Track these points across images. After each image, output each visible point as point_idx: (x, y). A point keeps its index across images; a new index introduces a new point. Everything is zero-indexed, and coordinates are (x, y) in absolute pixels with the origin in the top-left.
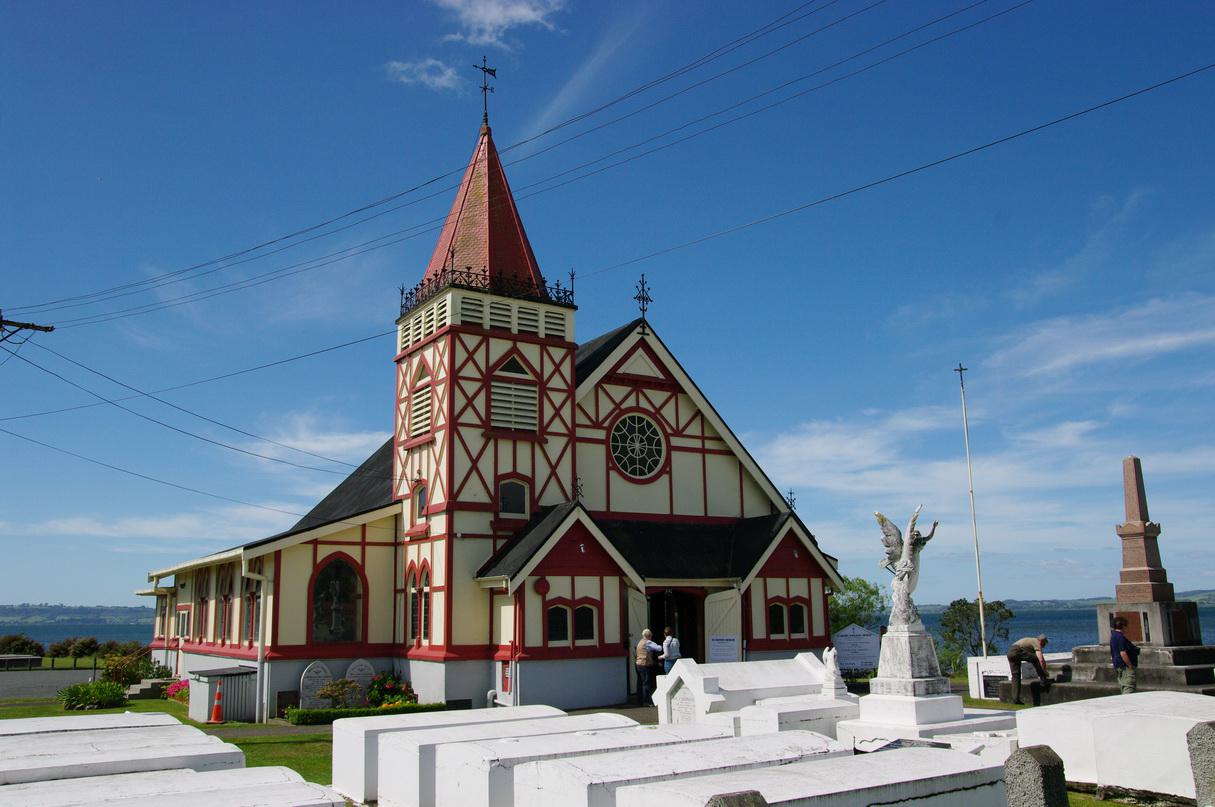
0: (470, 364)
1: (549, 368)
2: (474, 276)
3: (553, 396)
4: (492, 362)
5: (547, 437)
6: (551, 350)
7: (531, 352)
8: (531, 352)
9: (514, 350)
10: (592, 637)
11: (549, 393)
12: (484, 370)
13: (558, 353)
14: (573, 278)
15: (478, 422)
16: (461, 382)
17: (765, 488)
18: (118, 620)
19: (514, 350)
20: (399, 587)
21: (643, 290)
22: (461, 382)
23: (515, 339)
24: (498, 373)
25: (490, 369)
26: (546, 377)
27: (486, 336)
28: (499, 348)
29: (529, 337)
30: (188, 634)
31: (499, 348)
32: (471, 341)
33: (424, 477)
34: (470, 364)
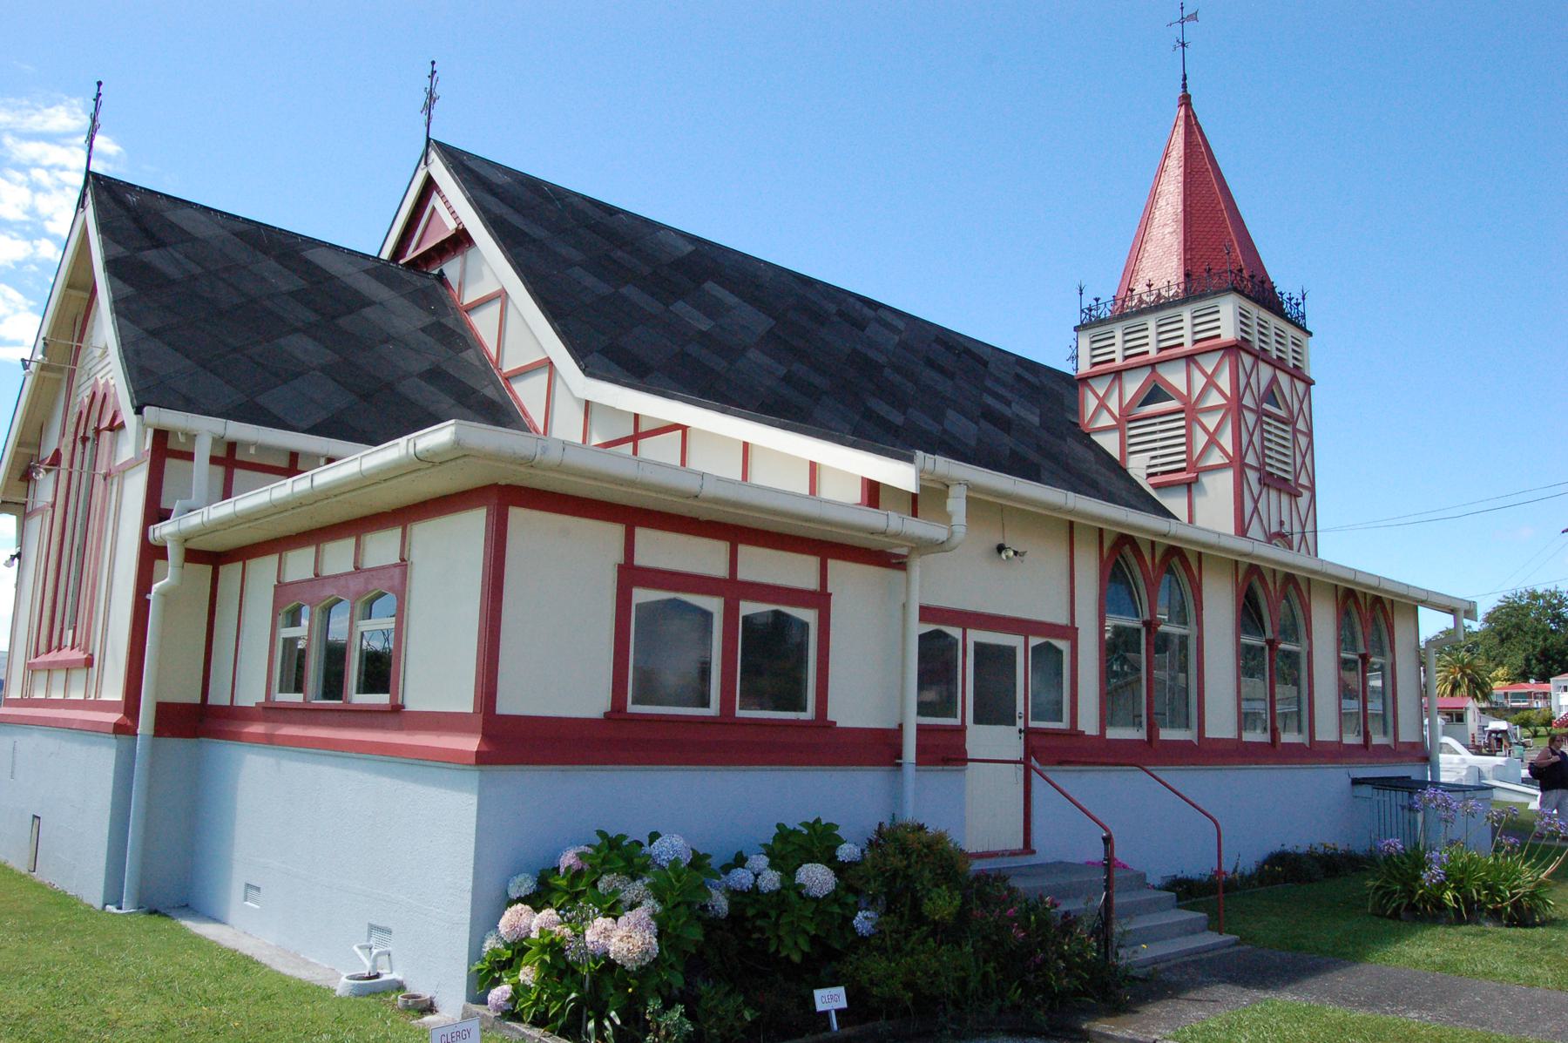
15: (1224, 402)
27: (1118, 374)
28: (1133, 385)
33: (1286, 528)
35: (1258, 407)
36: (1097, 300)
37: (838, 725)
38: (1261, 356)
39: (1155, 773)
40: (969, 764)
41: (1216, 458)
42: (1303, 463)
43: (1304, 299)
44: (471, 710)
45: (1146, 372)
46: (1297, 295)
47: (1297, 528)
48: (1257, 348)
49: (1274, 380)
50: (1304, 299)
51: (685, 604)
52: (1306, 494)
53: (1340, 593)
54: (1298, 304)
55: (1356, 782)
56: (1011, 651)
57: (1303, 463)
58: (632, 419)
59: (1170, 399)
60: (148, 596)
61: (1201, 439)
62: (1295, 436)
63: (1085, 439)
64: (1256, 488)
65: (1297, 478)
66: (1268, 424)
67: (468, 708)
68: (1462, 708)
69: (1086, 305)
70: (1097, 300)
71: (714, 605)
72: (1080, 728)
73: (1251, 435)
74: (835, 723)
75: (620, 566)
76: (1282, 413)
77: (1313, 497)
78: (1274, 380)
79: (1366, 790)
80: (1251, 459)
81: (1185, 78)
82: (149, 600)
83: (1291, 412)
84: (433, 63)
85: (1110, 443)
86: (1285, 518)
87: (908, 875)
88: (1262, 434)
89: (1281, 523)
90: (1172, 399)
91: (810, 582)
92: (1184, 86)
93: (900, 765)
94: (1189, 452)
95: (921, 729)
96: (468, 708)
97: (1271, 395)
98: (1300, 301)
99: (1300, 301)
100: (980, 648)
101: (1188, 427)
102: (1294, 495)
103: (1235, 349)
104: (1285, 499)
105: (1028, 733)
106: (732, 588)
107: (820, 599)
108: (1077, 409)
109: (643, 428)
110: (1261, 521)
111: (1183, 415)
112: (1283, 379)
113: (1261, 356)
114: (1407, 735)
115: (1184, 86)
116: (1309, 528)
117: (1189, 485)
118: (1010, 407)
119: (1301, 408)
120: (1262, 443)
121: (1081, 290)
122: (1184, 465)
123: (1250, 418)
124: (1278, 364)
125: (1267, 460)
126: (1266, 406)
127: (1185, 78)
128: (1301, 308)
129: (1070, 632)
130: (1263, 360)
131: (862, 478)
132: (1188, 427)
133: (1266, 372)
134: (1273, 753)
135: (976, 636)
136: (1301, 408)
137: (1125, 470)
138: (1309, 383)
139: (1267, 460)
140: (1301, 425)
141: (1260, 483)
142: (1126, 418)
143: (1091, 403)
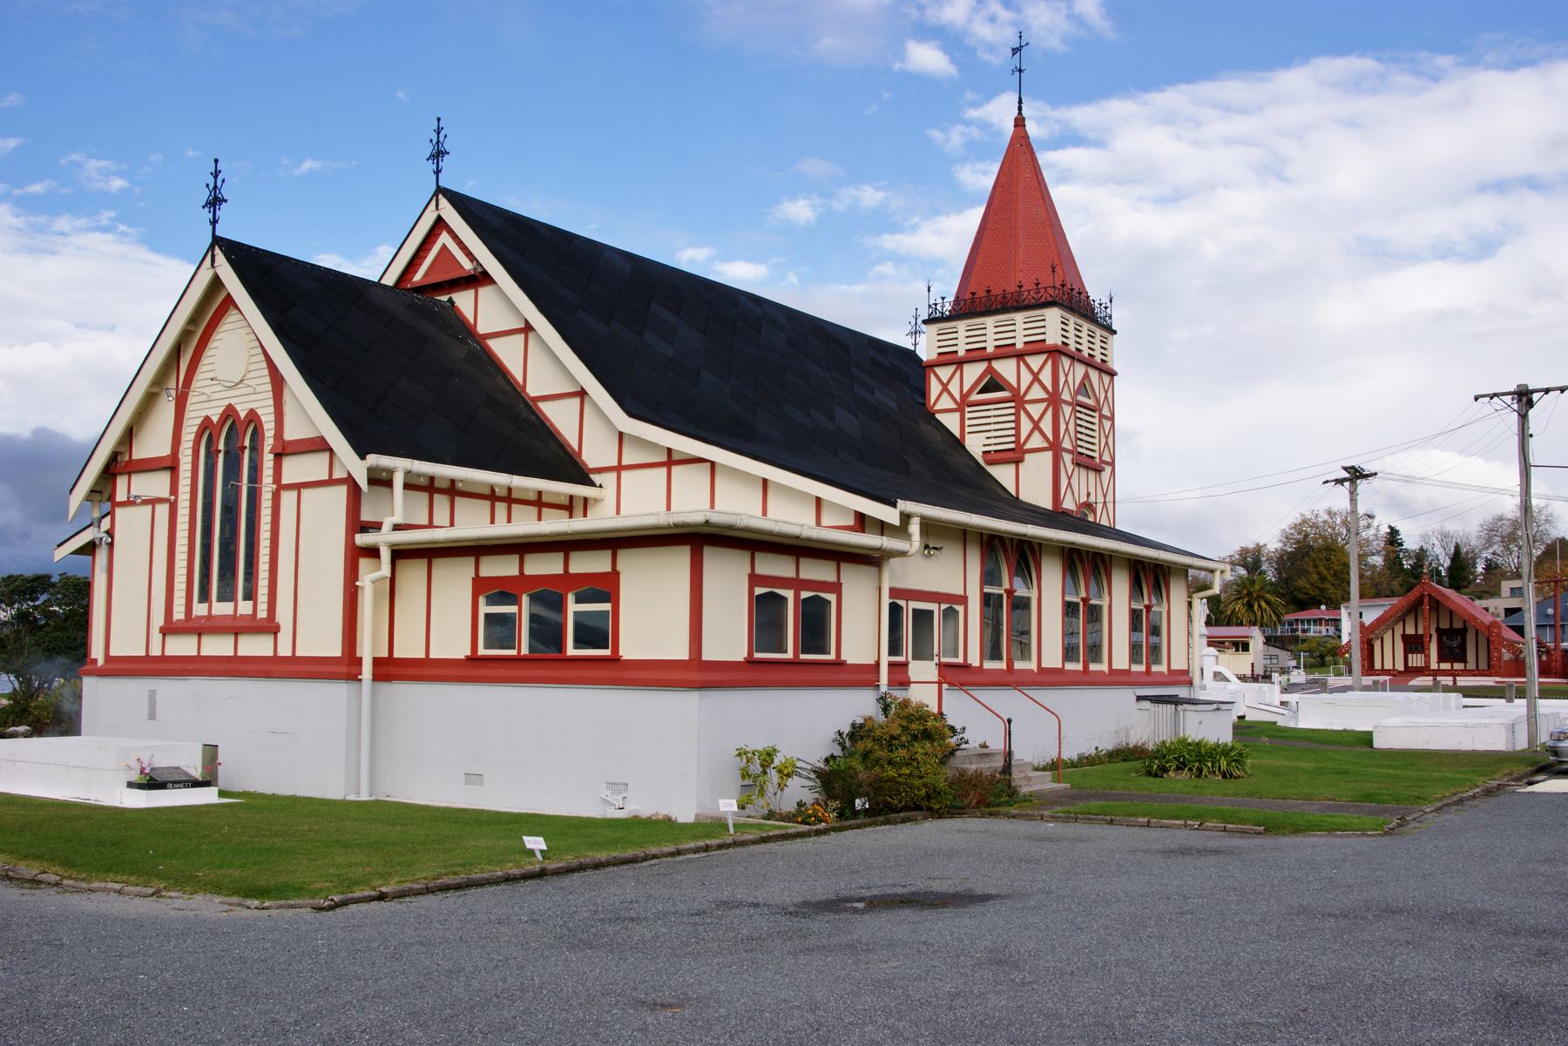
0: (1036, 386)
1: (1026, 378)
2: (1042, 291)
3: (1032, 409)
5: (238, 615)
6: (1029, 359)
7: (1006, 369)
8: (1006, 369)
9: (990, 370)
10: (914, 610)
11: (1027, 406)
12: (958, 398)
13: (1035, 362)
14: (929, 291)
16: (1027, 406)
17: (1550, 687)
18: (548, 425)
19: (990, 370)
20: (664, 458)
21: (916, 324)
22: (1027, 406)
23: (989, 359)
24: (975, 397)
25: (964, 397)
26: (1023, 390)
27: (960, 363)
28: (973, 372)
29: (1005, 352)
30: (901, 530)
31: (973, 372)
32: (944, 373)
33: (1092, 499)
34: (1036, 386)
35: (1073, 399)
36: (943, 298)
38: (1075, 357)
39: (1025, 691)
40: (912, 685)
42: (1107, 443)
43: (1111, 302)
44: (339, 654)
45: (983, 366)
46: (1105, 300)
47: (1100, 499)
48: (1074, 350)
50: (1111, 302)
51: (776, 594)
52: (1108, 469)
53: (1132, 563)
54: (1106, 308)
55: (1139, 698)
56: (931, 613)
57: (1107, 443)
59: (1002, 389)
61: (1026, 426)
62: (1100, 422)
63: (930, 416)
64: (1070, 467)
65: (1101, 456)
66: (1080, 412)
67: (338, 653)
68: (1248, 637)
69: (932, 302)
70: (943, 298)
71: (789, 594)
72: (843, 658)
73: (1067, 424)
75: (749, 575)
76: (1091, 402)
77: (1113, 470)
78: (1086, 376)
79: (1146, 704)
80: (1067, 444)
83: (1098, 401)
84: (439, 119)
85: (951, 422)
86: (1092, 491)
88: (1075, 421)
89: (1088, 495)
90: (1005, 390)
91: (832, 578)
92: (1020, 109)
93: (878, 686)
94: (1017, 435)
95: (891, 665)
96: (338, 653)
97: (1084, 387)
98: (1108, 304)
99: (1108, 304)
102: (1098, 471)
103: (1057, 353)
104: (1092, 475)
105: (941, 666)
106: (797, 584)
107: (836, 588)
108: (923, 392)
109: (675, 457)
110: (1073, 494)
111: (1013, 404)
112: (1094, 375)
113: (1075, 357)
114: (1178, 664)
115: (1020, 109)
116: (1109, 498)
118: (874, 394)
119: (1106, 397)
120: (1076, 429)
121: (929, 288)
122: (1012, 446)
123: (1067, 410)
124: (1089, 363)
125: (1079, 443)
126: (1081, 398)
128: (1108, 311)
129: (963, 600)
130: (1078, 360)
131: (855, 511)
132: (1017, 415)
133: (1080, 370)
134: (1086, 680)
135: (914, 605)
136: (1106, 397)
137: (964, 447)
138: (1112, 374)
139: (1079, 443)
140: (1106, 412)
141: (1073, 463)
142: (963, 404)
143: (935, 388)
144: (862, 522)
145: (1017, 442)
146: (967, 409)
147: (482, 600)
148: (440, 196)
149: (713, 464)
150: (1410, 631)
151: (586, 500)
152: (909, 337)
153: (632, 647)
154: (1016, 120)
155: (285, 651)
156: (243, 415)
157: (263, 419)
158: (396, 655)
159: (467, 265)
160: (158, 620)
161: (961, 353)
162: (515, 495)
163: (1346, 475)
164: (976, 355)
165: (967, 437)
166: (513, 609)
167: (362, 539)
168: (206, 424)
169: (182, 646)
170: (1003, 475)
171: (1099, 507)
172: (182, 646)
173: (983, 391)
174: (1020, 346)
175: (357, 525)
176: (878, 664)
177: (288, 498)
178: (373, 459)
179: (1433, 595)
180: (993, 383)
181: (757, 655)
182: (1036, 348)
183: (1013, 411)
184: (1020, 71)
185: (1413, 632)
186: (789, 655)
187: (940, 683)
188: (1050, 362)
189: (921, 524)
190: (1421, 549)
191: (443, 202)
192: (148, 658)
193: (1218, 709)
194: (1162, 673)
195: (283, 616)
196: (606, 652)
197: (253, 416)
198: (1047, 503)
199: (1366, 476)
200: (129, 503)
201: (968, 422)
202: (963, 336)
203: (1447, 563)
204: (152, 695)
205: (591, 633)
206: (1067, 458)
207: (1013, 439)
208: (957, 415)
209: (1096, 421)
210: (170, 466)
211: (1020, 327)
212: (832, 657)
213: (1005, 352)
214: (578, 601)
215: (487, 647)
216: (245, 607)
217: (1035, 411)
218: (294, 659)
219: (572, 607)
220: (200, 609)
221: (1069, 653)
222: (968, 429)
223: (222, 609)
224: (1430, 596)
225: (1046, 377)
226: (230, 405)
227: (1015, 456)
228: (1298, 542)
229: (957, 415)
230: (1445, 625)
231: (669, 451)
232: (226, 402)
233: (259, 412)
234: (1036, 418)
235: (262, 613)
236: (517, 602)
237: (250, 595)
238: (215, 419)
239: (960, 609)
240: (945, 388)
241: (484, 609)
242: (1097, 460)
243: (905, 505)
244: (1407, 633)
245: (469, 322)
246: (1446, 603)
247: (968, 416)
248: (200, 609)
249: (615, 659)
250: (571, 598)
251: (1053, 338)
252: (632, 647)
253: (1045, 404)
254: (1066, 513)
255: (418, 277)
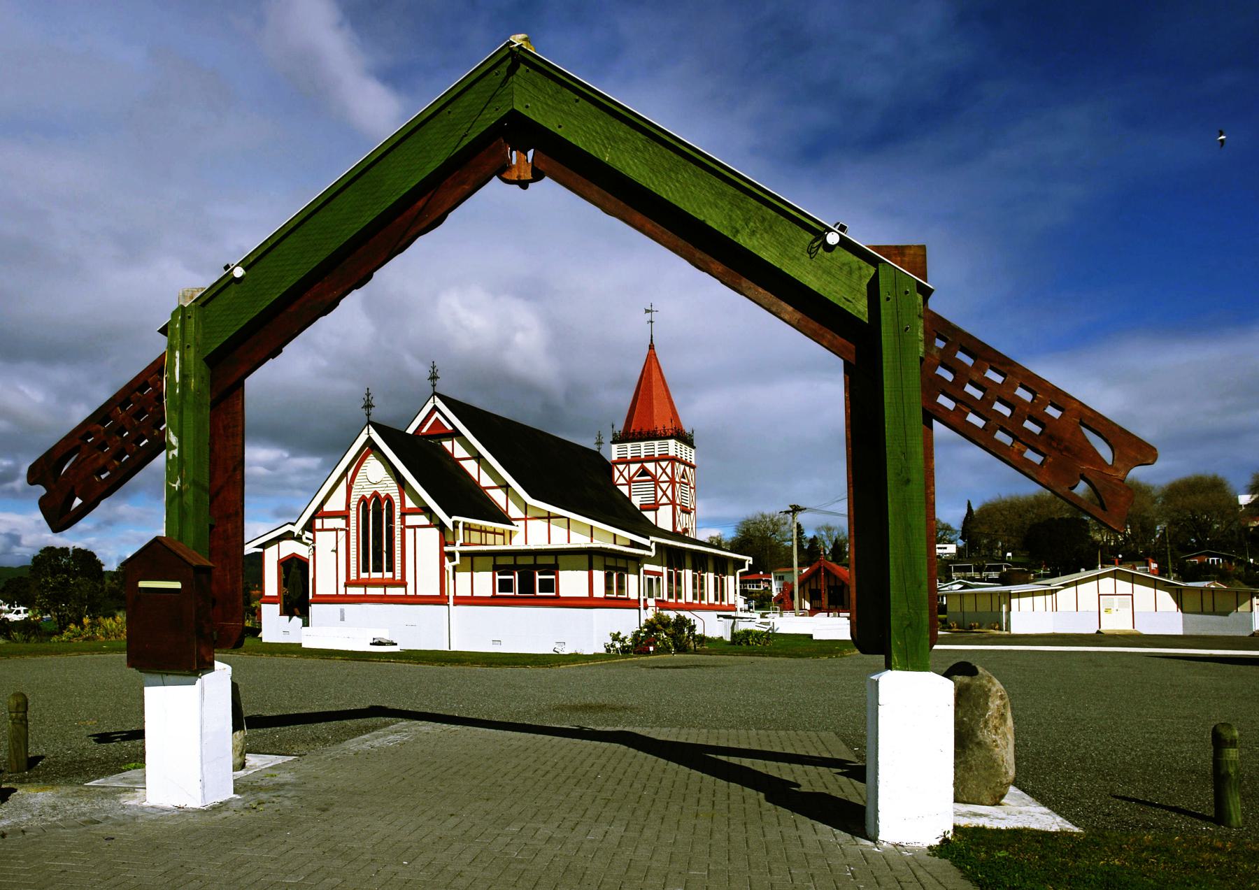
0: (664, 475)
1: (660, 471)
4: (631, 475)
6: (661, 463)
7: (650, 466)
8: (650, 466)
9: (642, 467)
12: (627, 478)
13: (664, 464)
15: (668, 480)
19: (642, 467)
23: (642, 461)
24: (635, 478)
29: (650, 459)
31: (634, 467)
32: (621, 467)
33: (687, 527)
37: (303, 646)
41: (665, 500)
45: (639, 465)
46: (691, 433)
47: (690, 527)
49: (685, 470)
55: (719, 616)
56: (652, 579)
58: (590, 528)
59: (648, 475)
60: (1083, 570)
61: (660, 493)
63: (615, 486)
64: (679, 512)
74: (300, 644)
76: (686, 481)
78: (685, 470)
79: (721, 619)
80: (678, 502)
81: (652, 337)
82: (1080, 572)
85: (625, 490)
86: (687, 522)
87: (780, 579)
91: (625, 566)
92: (652, 340)
94: (656, 497)
100: (648, 578)
101: (655, 488)
102: (689, 513)
105: (656, 600)
109: (551, 515)
111: (653, 483)
112: (687, 468)
114: (732, 602)
117: (656, 510)
122: (653, 502)
127: (652, 337)
132: (655, 488)
133: (682, 467)
142: (630, 482)
143: (617, 474)
144: (633, 544)
145: (656, 500)
146: (632, 484)
147: (497, 574)
148: (435, 397)
149: (569, 519)
150: (813, 587)
151: (511, 532)
152: (364, 409)
153: (565, 591)
154: (650, 346)
155: (411, 592)
156: (383, 496)
157: (394, 498)
158: (475, 595)
159: (450, 428)
160: (342, 580)
161: (629, 458)
162: (472, 527)
163: (791, 509)
164: (636, 460)
165: (632, 497)
166: (512, 577)
167: (446, 549)
168: (363, 499)
169: (352, 591)
170: (650, 515)
171: (690, 530)
172: (352, 591)
173: (638, 476)
174: (656, 456)
175: (443, 543)
176: (639, 599)
177: (409, 532)
178: (455, 518)
179: (826, 567)
180: (645, 472)
181: (607, 595)
182: (664, 457)
183: (653, 486)
184: (652, 322)
185: (815, 588)
186: (615, 595)
187: (656, 607)
188: (670, 464)
189: (656, 545)
190: (815, 536)
191: (437, 399)
192: (337, 595)
193: (750, 621)
194: (705, 604)
195: (409, 578)
196: (554, 594)
197: (388, 497)
198: (670, 529)
199: (801, 510)
200: (323, 530)
201: (632, 490)
202: (629, 449)
203: (831, 547)
204: (342, 611)
205: (548, 586)
206: (678, 507)
207: (653, 499)
208: (627, 487)
209: (688, 489)
210: (345, 515)
211: (656, 447)
212: (626, 596)
213: (650, 459)
214: (539, 575)
215: (540, 592)
216: (389, 575)
217: (664, 486)
218: (415, 596)
219: (538, 577)
220: (364, 575)
221: (695, 597)
222: (632, 494)
223: (378, 575)
224: (824, 568)
225: (669, 471)
226: (375, 492)
227: (655, 507)
228: (744, 532)
229: (627, 487)
230: (832, 584)
231: (549, 512)
232: (374, 490)
233: (392, 495)
234: (665, 490)
235: (398, 577)
236: (514, 575)
237: (391, 568)
238: (368, 497)
239: (661, 578)
240: (621, 474)
241: (498, 577)
242: (689, 508)
243: (652, 538)
244: (812, 588)
245: (450, 453)
246: (833, 572)
247: (632, 487)
248: (364, 575)
249: (558, 597)
250: (537, 573)
251: (672, 453)
252: (565, 591)
253: (668, 484)
254: (678, 533)
255: (424, 430)
